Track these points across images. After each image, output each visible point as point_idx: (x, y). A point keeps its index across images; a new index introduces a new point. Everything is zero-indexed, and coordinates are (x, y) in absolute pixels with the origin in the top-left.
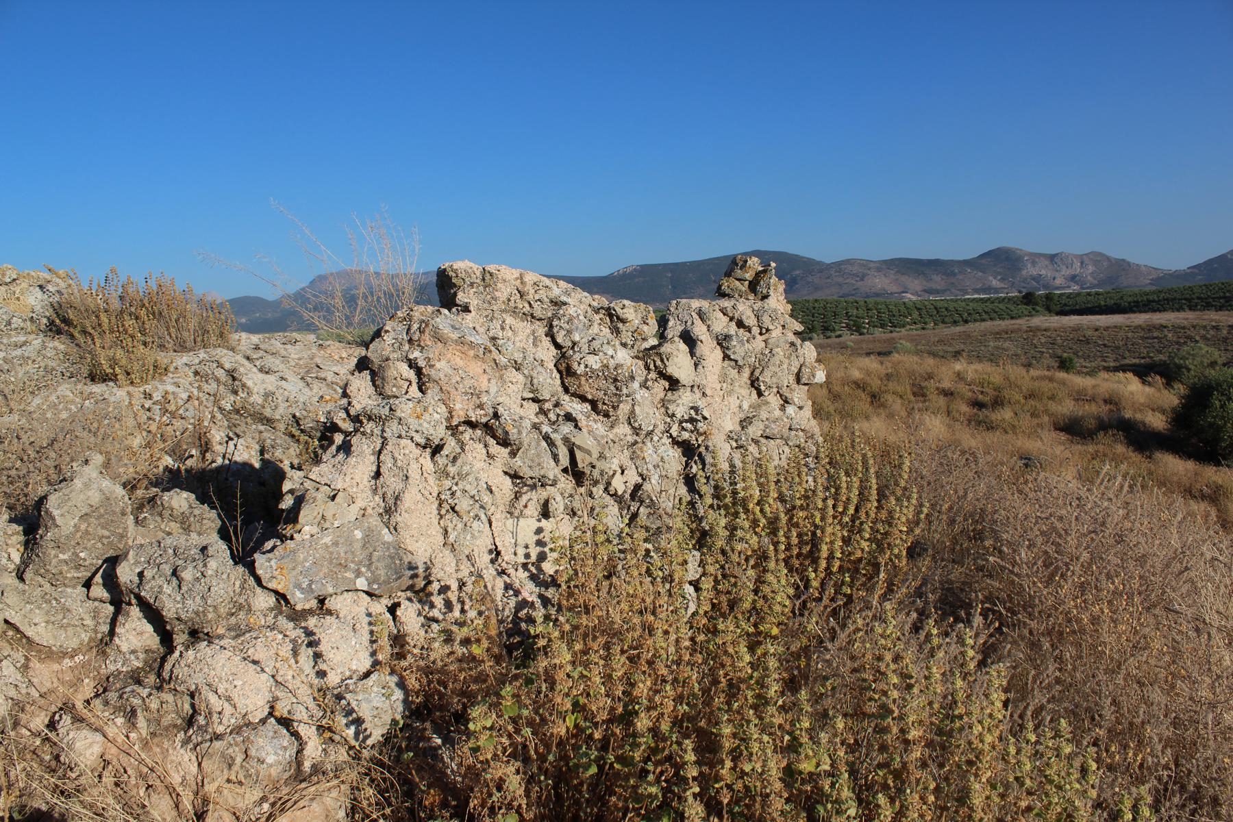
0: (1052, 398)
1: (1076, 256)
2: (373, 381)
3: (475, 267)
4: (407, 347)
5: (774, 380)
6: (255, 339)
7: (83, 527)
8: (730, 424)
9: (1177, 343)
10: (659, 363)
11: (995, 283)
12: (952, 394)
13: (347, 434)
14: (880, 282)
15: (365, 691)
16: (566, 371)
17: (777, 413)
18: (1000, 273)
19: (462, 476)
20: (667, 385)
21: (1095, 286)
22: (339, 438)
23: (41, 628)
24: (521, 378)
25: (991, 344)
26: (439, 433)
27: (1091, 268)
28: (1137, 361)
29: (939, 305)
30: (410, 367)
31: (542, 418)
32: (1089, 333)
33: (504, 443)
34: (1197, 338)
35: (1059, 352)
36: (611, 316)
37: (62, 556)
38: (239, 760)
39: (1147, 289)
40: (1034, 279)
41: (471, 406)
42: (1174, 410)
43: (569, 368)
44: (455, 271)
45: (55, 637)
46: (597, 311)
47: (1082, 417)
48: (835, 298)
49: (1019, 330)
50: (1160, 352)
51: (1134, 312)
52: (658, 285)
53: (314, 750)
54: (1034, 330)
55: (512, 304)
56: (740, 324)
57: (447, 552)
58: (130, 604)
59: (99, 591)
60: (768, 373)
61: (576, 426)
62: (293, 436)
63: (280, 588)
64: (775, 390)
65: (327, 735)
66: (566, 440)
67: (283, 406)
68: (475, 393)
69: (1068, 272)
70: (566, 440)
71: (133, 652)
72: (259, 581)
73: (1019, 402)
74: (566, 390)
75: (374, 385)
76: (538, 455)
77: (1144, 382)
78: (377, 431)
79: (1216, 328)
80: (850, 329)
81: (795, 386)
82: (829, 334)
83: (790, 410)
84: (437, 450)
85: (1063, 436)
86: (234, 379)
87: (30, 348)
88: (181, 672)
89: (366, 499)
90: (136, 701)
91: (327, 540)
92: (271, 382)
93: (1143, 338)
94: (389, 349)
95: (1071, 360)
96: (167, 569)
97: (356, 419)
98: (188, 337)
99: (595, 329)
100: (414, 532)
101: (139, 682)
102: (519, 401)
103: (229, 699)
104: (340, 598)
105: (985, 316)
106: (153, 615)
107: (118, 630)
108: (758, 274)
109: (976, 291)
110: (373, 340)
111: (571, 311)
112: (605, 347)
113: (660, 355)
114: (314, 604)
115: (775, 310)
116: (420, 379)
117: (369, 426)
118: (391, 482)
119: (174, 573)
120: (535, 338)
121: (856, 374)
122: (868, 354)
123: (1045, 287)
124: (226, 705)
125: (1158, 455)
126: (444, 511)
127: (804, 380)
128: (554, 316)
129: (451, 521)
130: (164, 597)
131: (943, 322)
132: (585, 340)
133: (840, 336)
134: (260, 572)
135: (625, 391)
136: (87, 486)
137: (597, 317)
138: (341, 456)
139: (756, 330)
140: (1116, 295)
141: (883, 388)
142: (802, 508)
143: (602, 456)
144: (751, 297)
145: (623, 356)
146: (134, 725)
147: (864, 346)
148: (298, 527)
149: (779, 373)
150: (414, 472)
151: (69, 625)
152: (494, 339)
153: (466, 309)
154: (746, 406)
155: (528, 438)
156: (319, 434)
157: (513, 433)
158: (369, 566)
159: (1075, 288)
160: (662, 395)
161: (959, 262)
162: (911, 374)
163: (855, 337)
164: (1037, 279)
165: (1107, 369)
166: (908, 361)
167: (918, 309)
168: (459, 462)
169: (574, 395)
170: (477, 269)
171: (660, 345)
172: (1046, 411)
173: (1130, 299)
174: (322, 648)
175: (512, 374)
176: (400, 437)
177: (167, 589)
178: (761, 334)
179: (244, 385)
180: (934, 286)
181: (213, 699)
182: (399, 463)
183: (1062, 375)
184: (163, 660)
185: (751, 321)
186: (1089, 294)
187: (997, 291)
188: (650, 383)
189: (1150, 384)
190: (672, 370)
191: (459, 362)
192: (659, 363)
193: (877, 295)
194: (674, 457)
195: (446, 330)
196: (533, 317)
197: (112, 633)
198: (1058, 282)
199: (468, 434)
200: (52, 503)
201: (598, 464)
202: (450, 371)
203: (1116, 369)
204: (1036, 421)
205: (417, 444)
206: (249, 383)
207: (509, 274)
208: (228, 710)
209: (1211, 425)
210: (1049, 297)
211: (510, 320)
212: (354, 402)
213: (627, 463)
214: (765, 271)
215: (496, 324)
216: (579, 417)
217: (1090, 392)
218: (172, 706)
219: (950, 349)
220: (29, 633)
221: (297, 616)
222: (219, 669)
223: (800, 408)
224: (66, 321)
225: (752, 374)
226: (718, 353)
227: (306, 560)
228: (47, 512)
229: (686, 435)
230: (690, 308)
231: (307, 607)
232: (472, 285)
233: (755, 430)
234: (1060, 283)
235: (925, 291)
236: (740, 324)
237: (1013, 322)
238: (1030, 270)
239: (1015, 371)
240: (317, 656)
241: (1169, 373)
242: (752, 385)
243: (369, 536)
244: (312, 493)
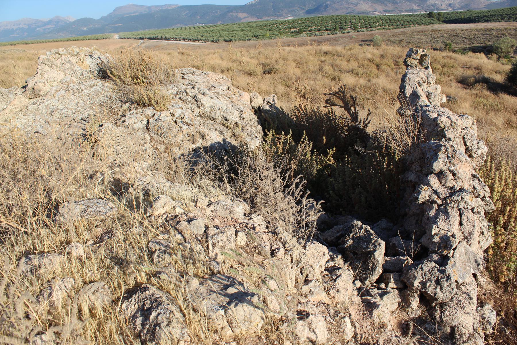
4: (449, 165)
9: (497, 37)
11: (415, 7)
18: (417, 3)
21: (459, 9)
25: (416, 37)
28: (479, 45)
29: (391, 17)
32: (459, 32)
34: (507, 34)
35: (445, 41)
39: (484, 10)
40: (432, 5)
47: (469, 77)
49: (428, 30)
50: (489, 41)
62: (224, 125)
85: (460, 85)
87: (98, 87)
93: (482, 35)
105: (411, 23)
109: (407, 11)
121: (369, 56)
123: (437, 9)
133: (349, 33)
141: (381, 62)
147: (360, 37)
159: (450, 10)
162: (392, 55)
167: (382, 20)
172: (453, 74)
173: (475, 15)
179: (202, 104)
182: (470, 221)
186: (457, 13)
187: (416, 11)
193: (363, 13)
198: (443, 7)
206: (204, 103)
217: (468, 64)
219: (398, 39)
235: (384, 11)
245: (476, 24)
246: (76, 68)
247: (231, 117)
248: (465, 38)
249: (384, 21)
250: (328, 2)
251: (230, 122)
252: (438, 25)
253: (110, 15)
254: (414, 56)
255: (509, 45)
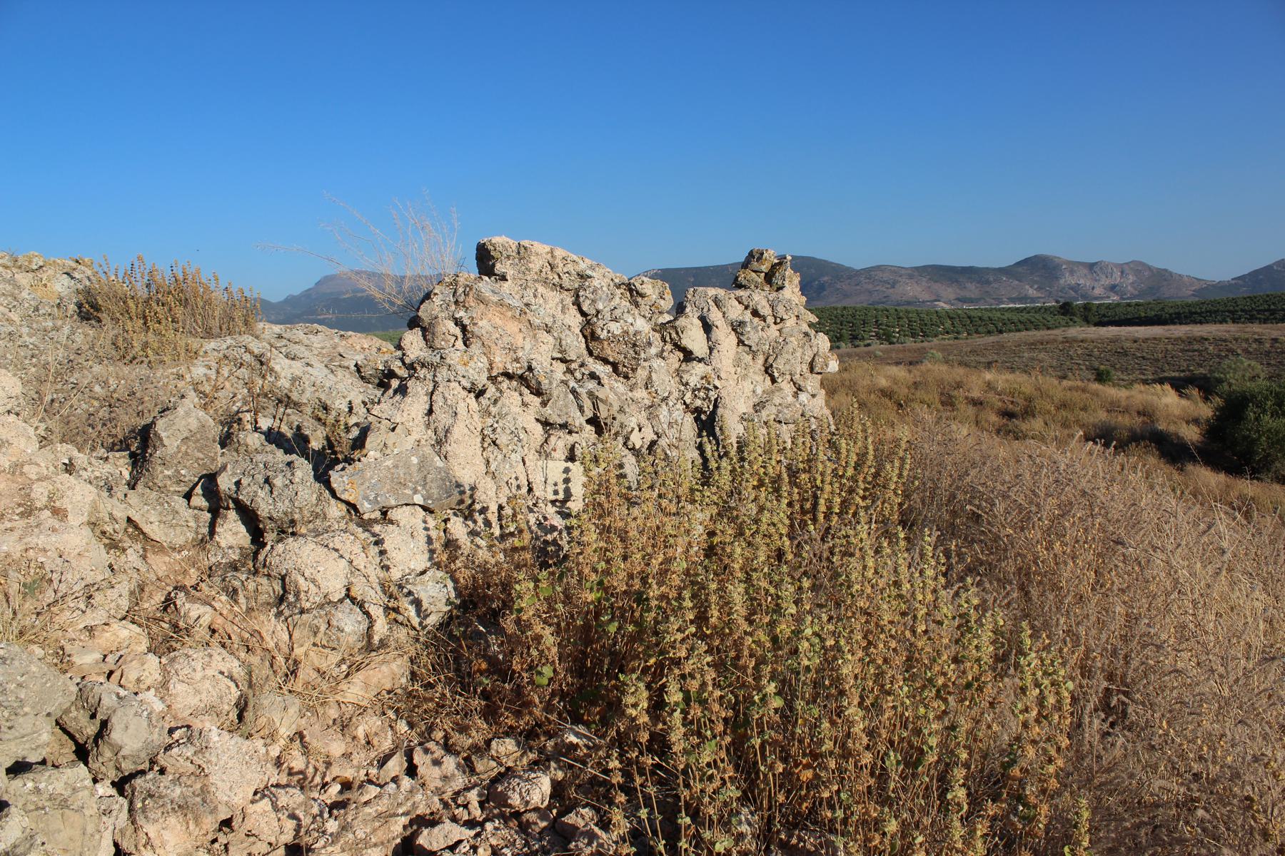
0: (1084, 409)
1: (1117, 266)
2: (424, 337)
3: (511, 242)
4: (453, 307)
5: (788, 367)
6: (277, 329)
7: (183, 449)
8: (744, 407)
9: (1219, 356)
10: (674, 335)
11: (1031, 292)
12: (981, 403)
13: (402, 379)
14: (913, 290)
15: (423, 583)
16: (590, 336)
17: (790, 399)
18: (1036, 282)
19: (501, 416)
20: (681, 356)
21: (1135, 297)
22: (395, 383)
23: (155, 526)
24: (551, 339)
25: (1026, 355)
26: (482, 380)
27: (1131, 278)
28: (1176, 374)
29: (972, 314)
30: (456, 324)
31: (569, 376)
33: (538, 392)
34: (1239, 351)
35: (1096, 364)
36: (631, 291)
37: (167, 472)
38: (323, 629)
39: (1190, 301)
40: (1072, 288)
41: (509, 360)
42: (1208, 421)
43: (593, 333)
44: (493, 245)
45: (166, 535)
46: (618, 287)
47: (1115, 428)
48: (865, 305)
49: (1055, 341)
51: (1174, 323)
52: (681, 282)
53: (381, 627)
54: (1067, 340)
55: (543, 274)
56: (755, 313)
57: (489, 479)
58: (228, 508)
59: (199, 500)
60: (781, 361)
61: (599, 383)
62: (319, 420)
63: (351, 499)
64: (788, 377)
65: (393, 615)
66: (591, 394)
67: (309, 390)
68: (512, 349)
69: (1108, 282)
70: (591, 394)
71: (230, 547)
72: (333, 493)
73: (1049, 412)
74: (591, 353)
75: (425, 339)
76: (566, 406)
77: (1181, 395)
78: (429, 376)
79: (1259, 341)
80: (879, 338)
81: (808, 375)
82: (857, 342)
83: (803, 397)
84: (480, 394)
86: (262, 363)
88: (274, 560)
89: (420, 432)
90: (237, 584)
91: (389, 463)
92: (297, 368)
93: (1182, 351)
94: (438, 309)
95: (1108, 372)
96: (260, 479)
97: (411, 367)
98: (215, 324)
99: (617, 300)
100: (461, 460)
101: (236, 569)
102: (549, 360)
103: (314, 581)
104: (400, 510)
105: (1021, 326)
106: (249, 517)
107: (218, 530)
108: (773, 266)
109: (1012, 300)
110: (422, 302)
111: (596, 283)
112: (626, 315)
113: (675, 328)
114: (377, 515)
115: (790, 301)
116: (464, 335)
117: (422, 372)
118: (442, 418)
119: (267, 481)
120: (563, 307)
121: (883, 382)
122: (897, 364)
123: (1084, 297)
124: (312, 585)
125: (1190, 467)
126: (486, 445)
127: (817, 369)
128: (581, 287)
129: (492, 453)
130: (259, 500)
131: (977, 332)
132: (608, 309)
133: (869, 345)
134: (334, 485)
135: (643, 355)
136: (188, 414)
137: (618, 292)
138: (398, 397)
139: (770, 320)
140: (1157, 307)
142: (804, 471)
143: (621, 410)
144: (767, 288)
145: (642, 325)
146: (236, 602)
147: (894, 355)
148: (365, 451)
149: (793, 361)
150: (461, 409)
151: (177, 525)
152: (527, 305)
153: (503, 278)
154: (759, 391)
155: (557, 392)
156: (377, 381)
157: (545, 382)
158: (424, 486)
159: (1114, 298)
160: (677, 365)
161: (995, 269)
162: (940, 383)
163: (885, 346)
164: (1075, 288)
165: (1145, 382)
166: (936, 369)
167: (951, 318)
168: (499, 403)
169: (597, 358)
170: (513, 244)
171: (676, 319)
173: (1171, 311)
174: (387, 545)
175: (543, 335)
176: (449, 381)
177: (261, 494)
178: (775, 323)
179: (272, 370)
180: (968, 294)
181: (301, 581)
182: (449, 402)
183: (1096, 386)
184: (256, 554)
185: (765, 310)
186: (1129, 305)
187: (1033, 300)
188: (665, 354)
189: (1187, 397)
190: (686, 342)
191: (498, 322)
192: (674, 335)
193: (909, 303)
194: (689, 424)
195: (487, 294)
196: (562, 287)
197: (212, 532)
198: (1097, 292)
199: (505, 384)
200: (161, 425)
201: (619, 417)
202: (491, 329)
203: (1154, 381)
204: (1066, 432)
205: (464, 388)
206: (277, 368)
207: (541, 248)
208: (313, 589)
209: (1245, 438)
210: (1087, 308)
211: (541, 289)
212: (408, 353)
213: (644, 422)
214: (780, 264)
215: (530, 292)
216: (602, 376)
217: (1123, 403)
218: (269, 588)
219: (983, 360)
220: (145, 530)
221: (366, 525)
222: (305, 558)
223: (813, 396)
224: (96, 307)
225: (766, 360)
226: (733, 339)
227: (372, 478)
228: (156, 434)
229: (698, 403)
230: (706, 295)
231: (373, 517)
232: (508, 257)
233: (768, 413)
234: (1100, 293)
235: (958, 299)
236: (755, 313)
237: (1049, 332)
238: (1068, 280)
239: (1050, 383)
240: (382, 553)
241: (1207, 387)
242: (766, 372)
243: (422, 465)
244: (375, 425)
245: (1166, 327)
246: (25, 294)
247: (337, 403)
248: (1143, 358)
249: (957, 322)
250: (826, 278)
251: (334, 413)
252: (1078, 328)
253: (307, 294)
254: (755, 265)
255: (1248, 375)
